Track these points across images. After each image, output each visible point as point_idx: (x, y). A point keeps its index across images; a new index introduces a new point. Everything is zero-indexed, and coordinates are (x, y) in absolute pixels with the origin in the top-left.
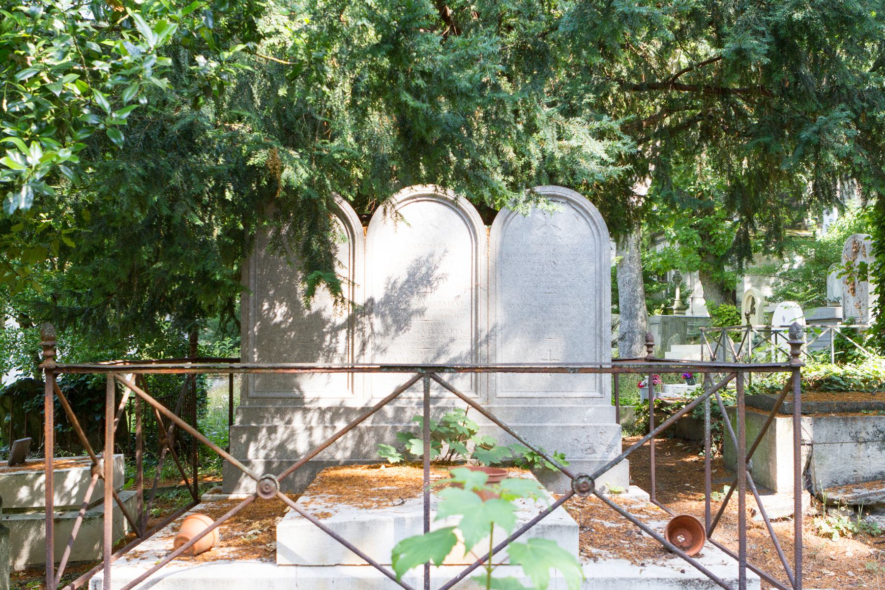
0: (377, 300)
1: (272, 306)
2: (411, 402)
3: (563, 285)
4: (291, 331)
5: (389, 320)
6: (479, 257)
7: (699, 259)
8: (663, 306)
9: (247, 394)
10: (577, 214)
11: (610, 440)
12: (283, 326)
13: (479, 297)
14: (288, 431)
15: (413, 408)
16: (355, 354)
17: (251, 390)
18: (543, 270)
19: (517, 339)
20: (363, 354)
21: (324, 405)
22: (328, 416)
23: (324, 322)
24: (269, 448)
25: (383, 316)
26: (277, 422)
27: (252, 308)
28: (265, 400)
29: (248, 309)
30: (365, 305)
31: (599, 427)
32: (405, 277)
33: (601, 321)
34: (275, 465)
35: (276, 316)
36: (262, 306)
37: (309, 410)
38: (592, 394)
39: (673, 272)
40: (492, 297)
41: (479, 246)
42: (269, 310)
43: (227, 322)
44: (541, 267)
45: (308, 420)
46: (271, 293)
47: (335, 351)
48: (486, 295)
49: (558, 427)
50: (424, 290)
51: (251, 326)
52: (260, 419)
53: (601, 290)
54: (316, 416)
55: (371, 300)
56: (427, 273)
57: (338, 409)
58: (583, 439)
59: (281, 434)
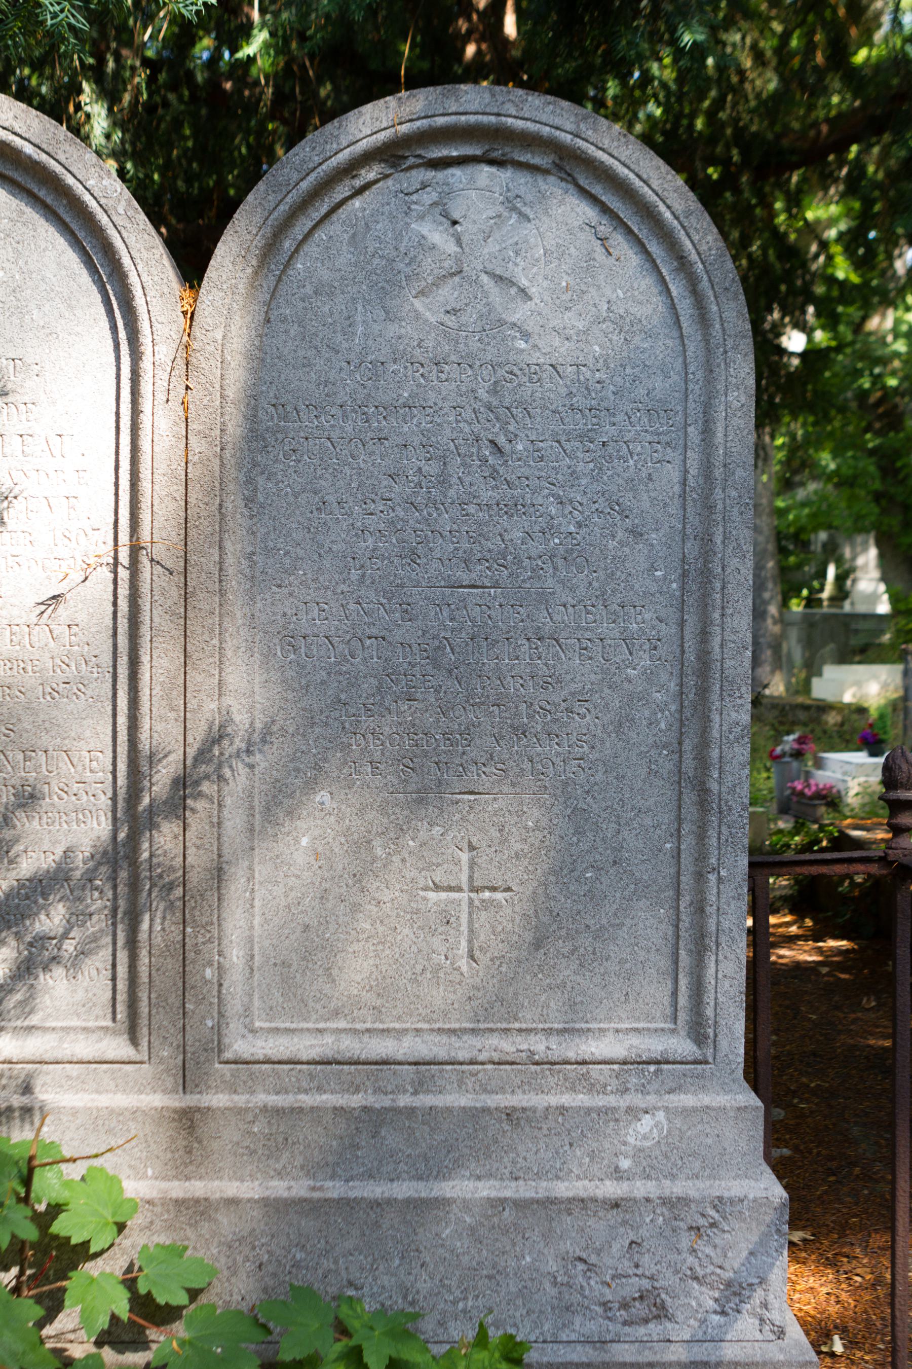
3: (535, 547)
6: (146, 419)
7: (876, 510)
8: (805, 592)
10: (605, 229)
11: (736, 1260)
13: (145, 603)
18: (443, 480)
19: (323, 796)
31: (684, 1201)
33: (706, 720)
38: (655, 1046)
39: (823, 536)
40: (203, 602)
41: (146, 364)
44: (432, 468)
48: (175, 593)
49: (500, 1203)
53: (706, 575)
58: (614, 1258)
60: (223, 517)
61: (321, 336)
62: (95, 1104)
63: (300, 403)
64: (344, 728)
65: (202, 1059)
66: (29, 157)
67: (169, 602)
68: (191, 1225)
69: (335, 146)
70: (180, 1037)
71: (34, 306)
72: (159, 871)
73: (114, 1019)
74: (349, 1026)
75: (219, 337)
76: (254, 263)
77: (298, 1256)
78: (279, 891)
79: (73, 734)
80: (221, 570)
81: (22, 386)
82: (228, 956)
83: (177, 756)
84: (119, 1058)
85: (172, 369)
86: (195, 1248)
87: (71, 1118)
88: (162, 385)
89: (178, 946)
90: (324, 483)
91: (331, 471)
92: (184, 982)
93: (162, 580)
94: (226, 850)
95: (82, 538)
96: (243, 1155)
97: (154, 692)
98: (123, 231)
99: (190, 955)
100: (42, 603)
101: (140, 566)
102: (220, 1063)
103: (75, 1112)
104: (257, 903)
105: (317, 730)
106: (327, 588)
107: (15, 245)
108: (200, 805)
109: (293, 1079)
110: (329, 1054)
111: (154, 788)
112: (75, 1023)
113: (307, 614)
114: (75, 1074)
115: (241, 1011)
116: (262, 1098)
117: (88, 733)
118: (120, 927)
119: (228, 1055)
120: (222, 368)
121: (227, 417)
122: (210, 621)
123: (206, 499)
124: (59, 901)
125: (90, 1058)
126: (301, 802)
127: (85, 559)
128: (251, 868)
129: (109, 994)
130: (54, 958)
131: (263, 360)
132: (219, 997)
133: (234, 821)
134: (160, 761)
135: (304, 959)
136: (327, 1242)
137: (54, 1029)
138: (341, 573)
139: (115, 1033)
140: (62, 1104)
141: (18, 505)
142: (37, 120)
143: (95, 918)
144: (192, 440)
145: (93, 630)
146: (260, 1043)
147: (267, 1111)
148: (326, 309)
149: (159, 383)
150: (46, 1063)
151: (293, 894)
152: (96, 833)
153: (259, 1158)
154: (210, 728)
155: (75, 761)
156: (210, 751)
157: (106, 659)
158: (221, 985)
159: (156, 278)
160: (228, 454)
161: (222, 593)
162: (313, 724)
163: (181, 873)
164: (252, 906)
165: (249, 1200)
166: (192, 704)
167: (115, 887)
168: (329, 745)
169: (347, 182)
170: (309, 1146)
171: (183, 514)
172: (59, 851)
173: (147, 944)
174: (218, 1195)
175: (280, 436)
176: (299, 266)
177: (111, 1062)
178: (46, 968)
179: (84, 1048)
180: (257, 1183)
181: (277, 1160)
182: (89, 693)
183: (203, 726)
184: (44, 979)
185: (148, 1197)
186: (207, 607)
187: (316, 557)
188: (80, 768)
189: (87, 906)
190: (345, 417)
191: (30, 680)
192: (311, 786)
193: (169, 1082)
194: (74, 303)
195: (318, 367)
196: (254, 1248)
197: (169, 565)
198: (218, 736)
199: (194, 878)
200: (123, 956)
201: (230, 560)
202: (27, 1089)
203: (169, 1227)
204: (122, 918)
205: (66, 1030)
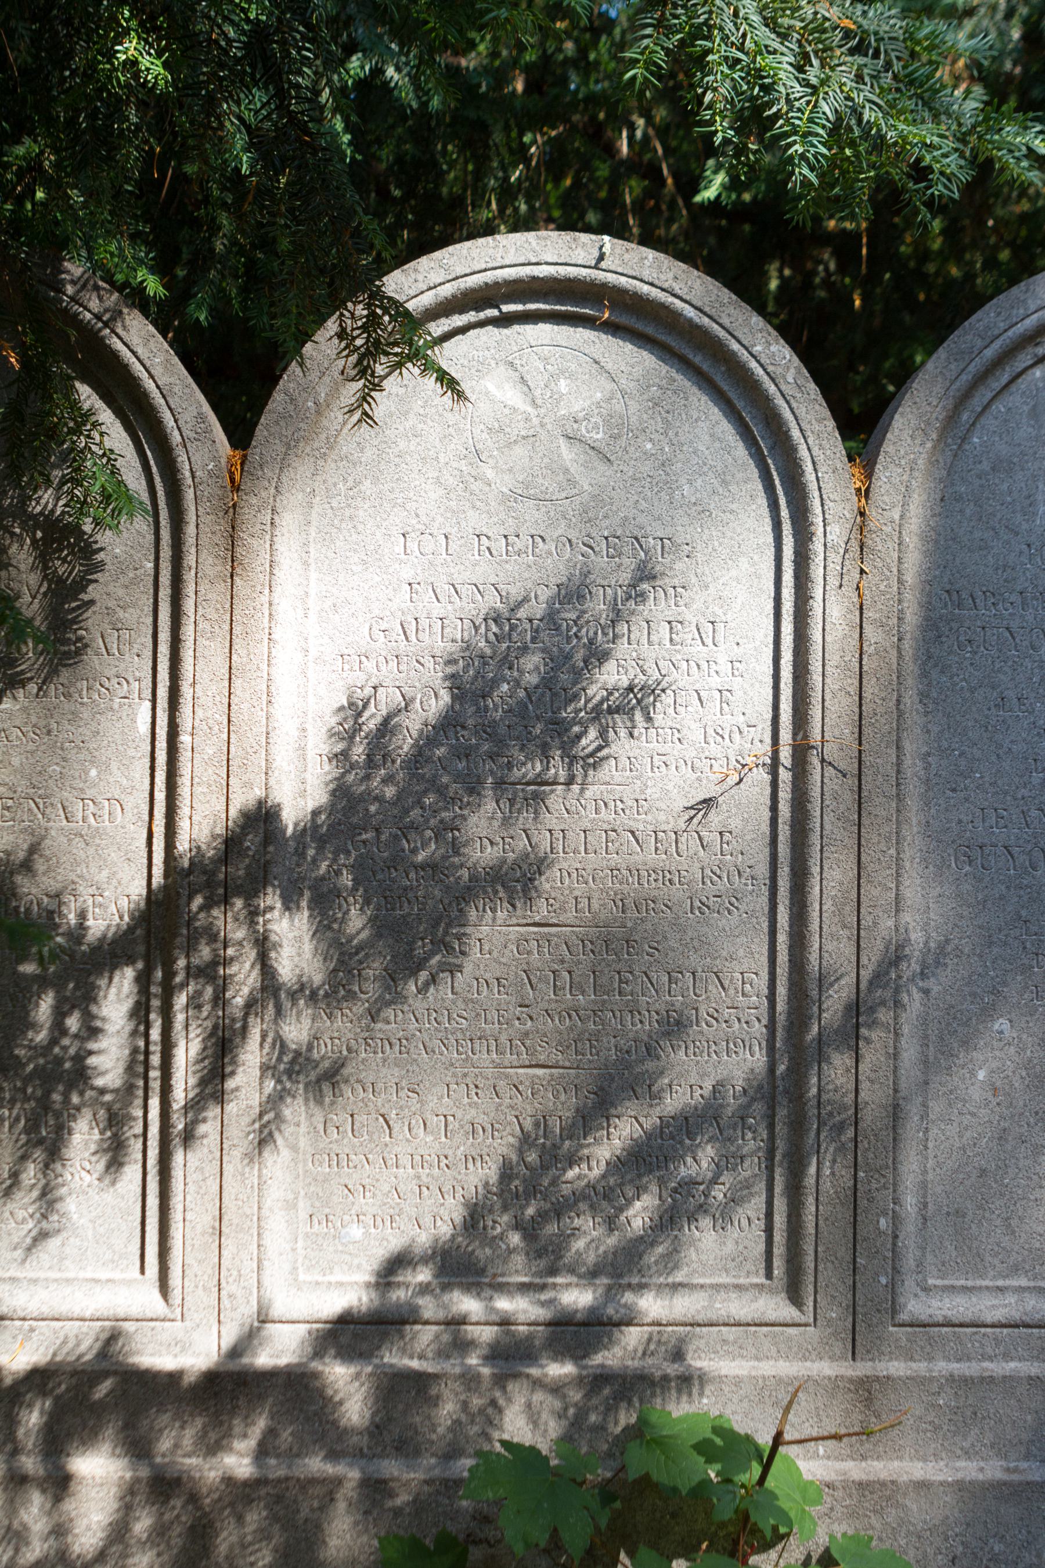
2: (461, 1345)
5: (356, 922)
6: (816, 606)
15: (470, 1380)
16: (179, 1096)
19: (1002, 1024)
20: (220, 1097)
25: (324, 903)
32: (433, 704)
47: (80, 1075)
48: (849, 798)
50: (534, 768)
55: (262, 818)
56: (548, 683)
60: (900, 714)
61: (999, 516)
62: (760, 1372)
63: (977, 589)
64: (1025, 948)
65: (875, 1321)
66: (690, 321)
67: (842, 807)
68: (875, 1511)
69: (1021, 311)
70: (850, 1296)
71: (684, 481)
72: (829, 1108)
73: (769, 1275)
74: (1032, 1284)
75: (897, 517)
76: (934, 436)
77: (996, 1548)
78: (952, 1130)
79: (724, 954)
80: (898, 772)
81: (671, 568)
82: (903, 1203)
83: (850, 980)
84: (782, 1320)
85: (846, 551)
86: (880, 1539)
87: (734, 1388)
88: (834, 568)
89: (849, 1192)
90: (1002, 677)
91: (1010, 663)
92: (855, 1234)
93: (834, 782)
94: (903, 1085)
95: (736, 736)
96: (925, 1431)
97: (824, 908)
98: (792, 401)
99: (863, 1203)
100: (692, 808)
101: (809, 768)
102: (894, 1325)
103: (738, 1381)
104: (930, 1145)
105: (995, 950)
106: (1006, 793)
107: (664, 415)
108: (875, 1035)
109: (977, 1344)
110: (1016, 1316)
111: (824, 1015)
112: (724, 1279)
113: (984, 821)
114: (731, 1338)
115: (913, 1267)
116: (942, 1367)
117: (741, 953)
118: (778, 1171)
119: (904, 1317)
120: (900, 551)
121: (906, 605)
122: (888, 829)
123: (883, 695)
124: (708, 1141)
125: (749, 1320)
126: (978, 1030)
127: (739, 758)
128: (924, 1105)
129: (762, 1247)
130: (701, 1206)
131: (945, 545)
132: (893, 1251)
133: (910, 1052)
134: (831, 985)
135: (980, 1207)
136: (1029, 1532)
137: (702, 1286)
138: (1022, 776)
139: (771, 1291)
140: (723, 1372)
141: (668, 699)
142: (699, 281)
143: (747, 1163)
144: (868, 629)
145: (748, 837)
146: (935, 1303)
147: (954, 1381)
148: (1005, 487)
149: (831, 566)
150: (699, 1325)
151: (968, 1134)
152: (749, 1064)
153: (944, 1435)
154: (887, 948)
155: (726, 983)
156: (887, 973)
157: (762, 870)
158: (896, 1237)
159: (828, 452)
160: (907, 645)
161: (899, 797)
162: (991, 944)
163: (853, 1111)
164: (926, 1148)
165: (941, 1484)
166: (867, 921)
167: (771, 1127)
168: (1009, 967)
169: (1030, 350)
170: (1001, 1421)
171: (857, 710)
172: (708, 1085)
173: (814, 1190)
174: (905, 1478)
175: (954, 625)
176: (976, 440)
177: (772, 1325)
178: (692, 1218)
179: (739, 1307)
180: (942, 1463)
181: (965, 1437)
182: (743, 907)
183: (880, 945)
184: (689, 1232)
185: (827, 1479)
186: (884, 813)
187: (994, 758)
188: (732, 992)
189: (739, 1147)
190: (1024, 605)
191: (677, 892)
192: (988, 1012)
193: (838, 1348)
194: (728, 478)
195: (995, 551)
196: (946, 1539)
197: (842, 766)
198: (895, 956)
199: (869, 1117)
200: (780, 1205)
201: (908, 761)
202: (678, 1355)
203: (852, 1514)
204: (782, 1162)
205: (717, 1287)
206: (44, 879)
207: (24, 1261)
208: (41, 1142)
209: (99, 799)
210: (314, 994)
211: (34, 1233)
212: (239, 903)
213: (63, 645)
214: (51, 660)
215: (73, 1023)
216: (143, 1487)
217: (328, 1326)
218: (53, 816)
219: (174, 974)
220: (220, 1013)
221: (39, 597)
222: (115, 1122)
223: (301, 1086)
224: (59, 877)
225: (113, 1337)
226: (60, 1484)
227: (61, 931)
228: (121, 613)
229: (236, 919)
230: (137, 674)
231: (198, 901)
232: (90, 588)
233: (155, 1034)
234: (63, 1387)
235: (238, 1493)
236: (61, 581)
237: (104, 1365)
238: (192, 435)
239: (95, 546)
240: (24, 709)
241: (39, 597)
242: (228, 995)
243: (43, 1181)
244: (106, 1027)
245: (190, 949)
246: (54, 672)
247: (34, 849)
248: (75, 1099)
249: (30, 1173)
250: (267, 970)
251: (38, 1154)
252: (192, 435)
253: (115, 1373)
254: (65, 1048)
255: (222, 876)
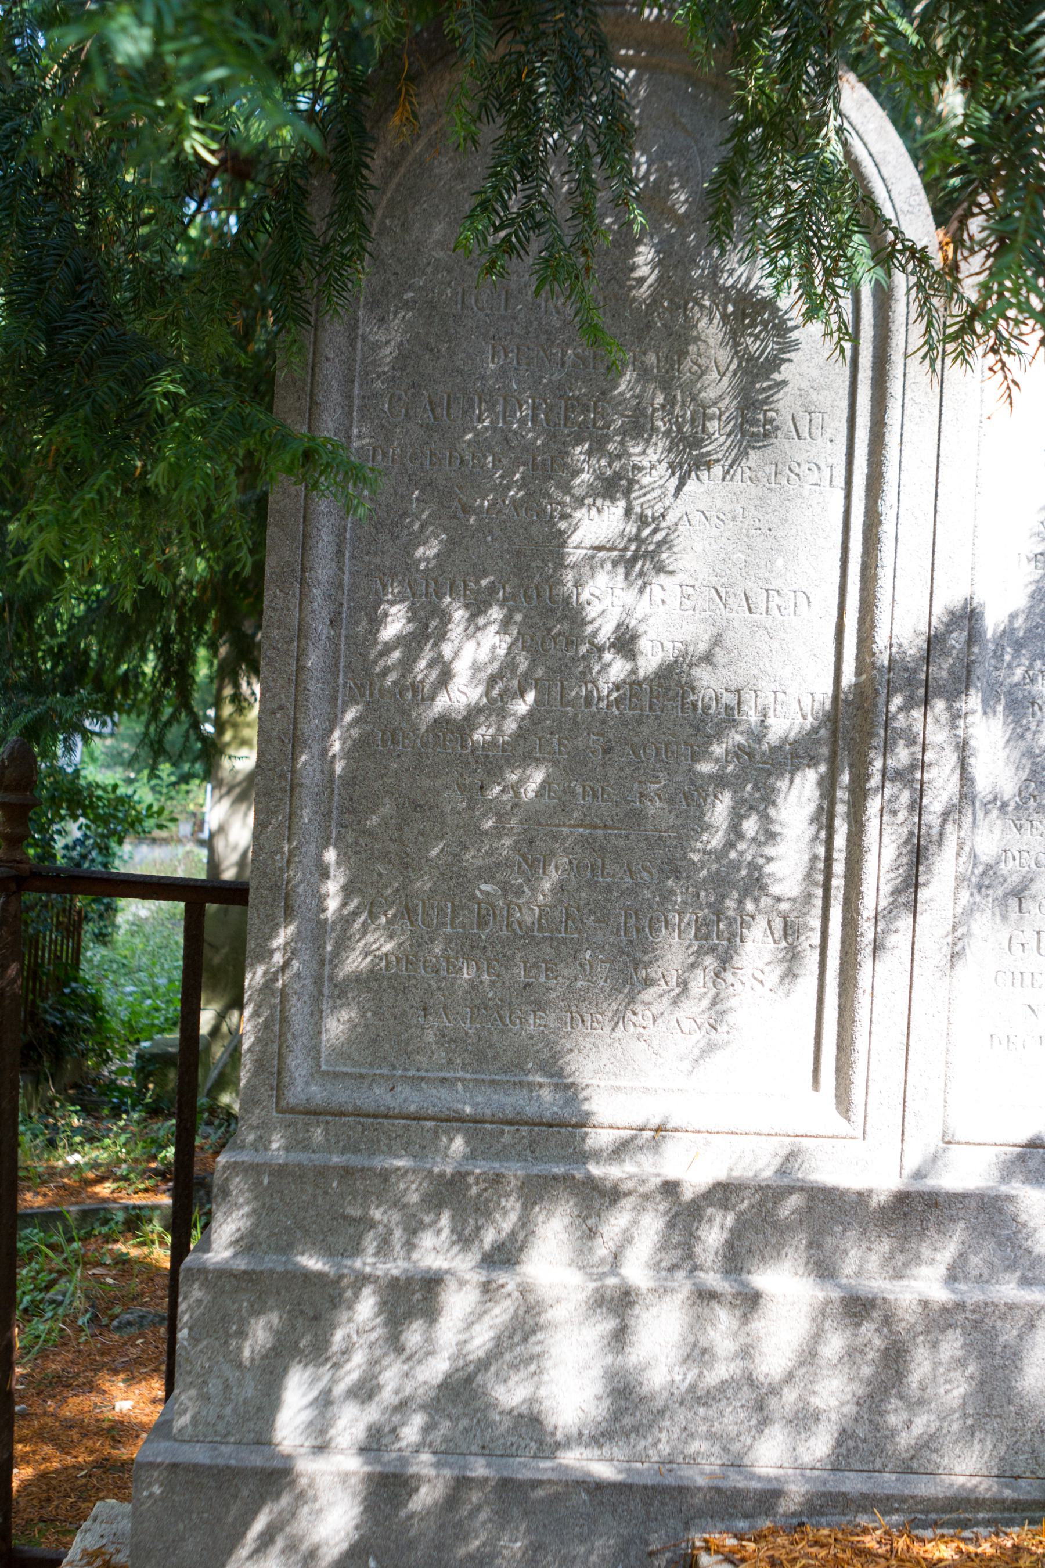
0: (993, 622)
1: (427, 630)
4: (529, 759)
9: (279, 1089)
12: (481, 734)
14: (501, 1313)
16: (868, 905)
17: (298, 1065)
21: (696, 1168)
22: (713, 1236)
23: (705, 724)
24: (387, 1396)
26: (434, 1251)
27: (321, 628)
28: (372, 1126)
29: (302, 632)
30: (934, 643)
34: (425, 1498)
35: (446, 676)
36: (377, 622)
37: (613, 1195)
42: (411, 644)
43: (168, 723)
45: (602, 1250)
46: (428, 551)
47: (755, 883)
51: (311, 724)
52: (343, 1233)
54: (650, 1227)
55: (968, 617)
57: (770, 1195)
59: (464, 1322)
206: (724, 672)
207: (691, 1072)
208: (713, 949)
209: (785, 590)
210: (1004, 806)
211: (702, 1044)
212: (939, 705)
213: (752, 426)
214: (740, 442)
215: (750, 826)
216: (836, 1308)
217: (1019, 1149)
218: (735, 607)
219: (868, 777)
220: (916, 820)
221: (729, 374)
222: (790, 930)
223: (990, 899)
224: (740, 671)
225: (792, 1156)
226: (750, 1301)
227: (740, 728)
228: (814, 396)
229: (937, 721)
230: (830, 460)
231: (897, 701)
232: (782, 368)
233: (840, 841)
234: (746, 1203)
235: (939, 1319)
236: (751, 358)
237: (786, 1181)
238: (906, 208)
239: (790, 324)
240: (709, 492)
241: (729, 374)
242: (925, 801)
243: (714, 991)
244: (785, 831)
245: (887, 749)
246: (744, 454)
247: (717, 641)
248: (750, 906)
249: (699, 982)
250: (965, 777)
251: (710, 962)
252: (906, 208)
253: (802, 1189)
254: (741, 854)
255: (923, 676)
